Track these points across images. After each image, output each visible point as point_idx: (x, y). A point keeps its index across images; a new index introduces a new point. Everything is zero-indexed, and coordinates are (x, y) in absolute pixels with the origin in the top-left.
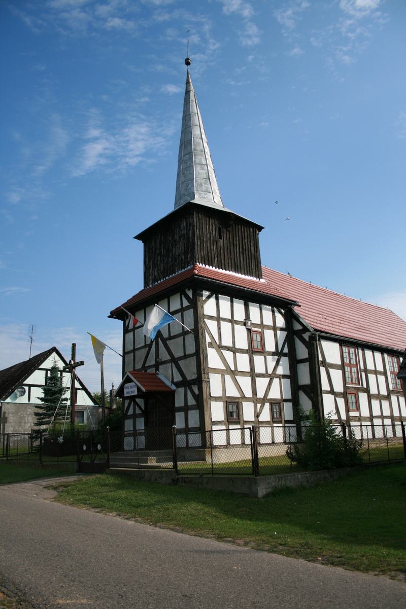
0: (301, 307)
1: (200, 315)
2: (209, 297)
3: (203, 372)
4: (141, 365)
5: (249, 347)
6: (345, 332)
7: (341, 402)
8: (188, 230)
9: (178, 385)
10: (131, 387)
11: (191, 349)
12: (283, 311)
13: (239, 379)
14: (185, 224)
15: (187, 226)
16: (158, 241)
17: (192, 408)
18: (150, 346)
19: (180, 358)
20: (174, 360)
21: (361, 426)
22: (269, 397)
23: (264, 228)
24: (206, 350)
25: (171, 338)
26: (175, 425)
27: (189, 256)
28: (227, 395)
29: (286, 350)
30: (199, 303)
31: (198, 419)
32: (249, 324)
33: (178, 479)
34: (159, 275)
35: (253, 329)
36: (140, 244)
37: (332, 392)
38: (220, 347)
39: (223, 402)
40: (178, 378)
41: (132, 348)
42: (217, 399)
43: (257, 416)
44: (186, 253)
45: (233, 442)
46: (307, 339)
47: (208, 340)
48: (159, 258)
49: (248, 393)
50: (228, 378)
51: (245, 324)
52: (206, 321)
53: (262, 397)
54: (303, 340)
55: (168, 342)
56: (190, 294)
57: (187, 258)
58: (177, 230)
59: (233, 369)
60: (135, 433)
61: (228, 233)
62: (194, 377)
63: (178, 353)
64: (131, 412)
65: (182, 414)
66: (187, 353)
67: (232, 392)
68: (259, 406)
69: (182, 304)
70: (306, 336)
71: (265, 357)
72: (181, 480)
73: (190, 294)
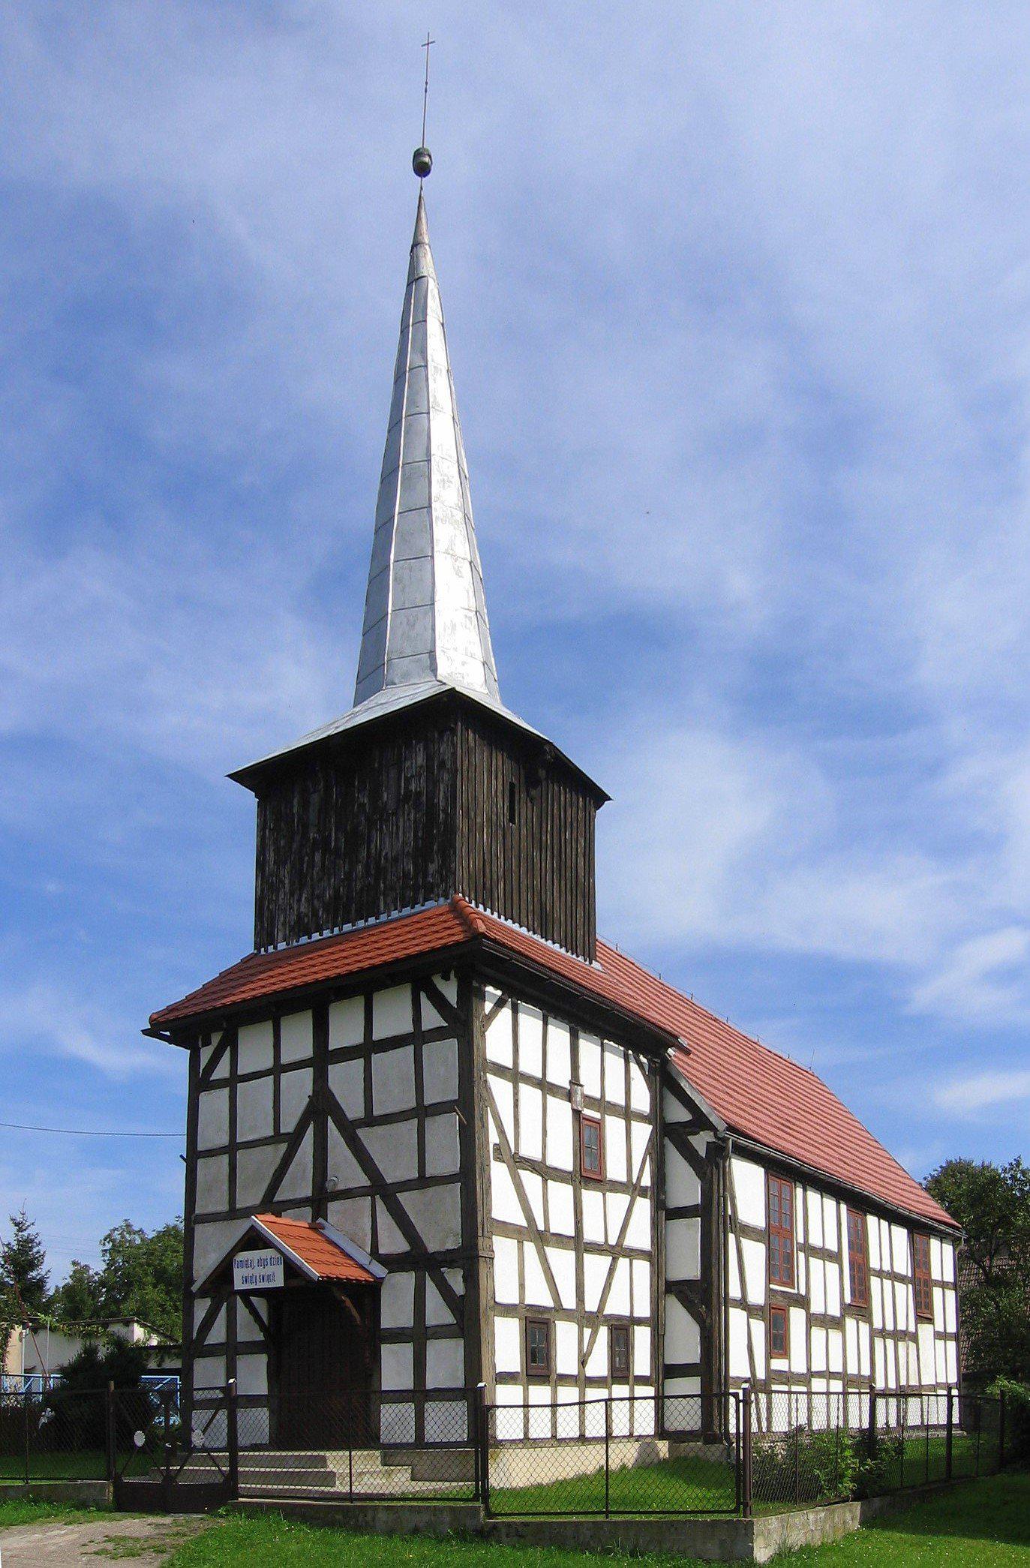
0: (691, 1056)
1: (477, 1060)
2: (500, 1004)
3: (480, 1234)
4: (261, 1194)
5: (574, 1165)
6: (773, 1138)
7: (759, 1328)
8: (433, 782)
9: (394, 1263)
10: (262, 1263)
11: (444, 1159)
12: (644, 1060)
13: (551, 1252)
14: (421, 759)
15: (429, 768)
16: (315, 799)
17: (441, 1332)
18: (294, 1140)
19: (406, 1186)
20: (381, 1189)
21: (632, 1399)
22: (607, 1311)
23: (610, 799)
24: (489, 1166)
25: (370, 1120)
26: (481, 1381)
27: (432, 868)
28: (527, 1302)
29: (646, 1181)
30: (477, 1024)
31: (462, 1367)
32: (579, 1098)
33: (495, 1526)
34: (315, 914)
35: (587, 1112)
36: (248, 799)
37: (743, 1304)
38: (518, 1163)
39: (520, 1319)
40: (393, 1242)
41: (224, 1140)
42: (508, 1310)
43: (583, 1362)
44: (422, 854)
45: (504, 1431)
46: (703, 1153)
47: (494, 1138)
48: (318, 857)
49: (569, 1302)
50: (530, 1247)
51: (569, 1096)
52: (490, 1077)
53: (595, 1309)
54: (689, 1153)
55: (362, 1133)
56: (450, 991)
57: (425, 875)
58: (393, 773)
59: (541, 1227)
60: (231, 1401)
61: (529, 804)
62: (453, 1243)
63: (397, 1168)
64: (217, 1335)
65: (407, 1350)
66: (430, 1172)
67: (539, 1296)
68: (587, 1332)
69: (417, 1019)
70: (700, 1142)
71: (604, 1195)
72: (504, 1530)
73: (450, 991)
